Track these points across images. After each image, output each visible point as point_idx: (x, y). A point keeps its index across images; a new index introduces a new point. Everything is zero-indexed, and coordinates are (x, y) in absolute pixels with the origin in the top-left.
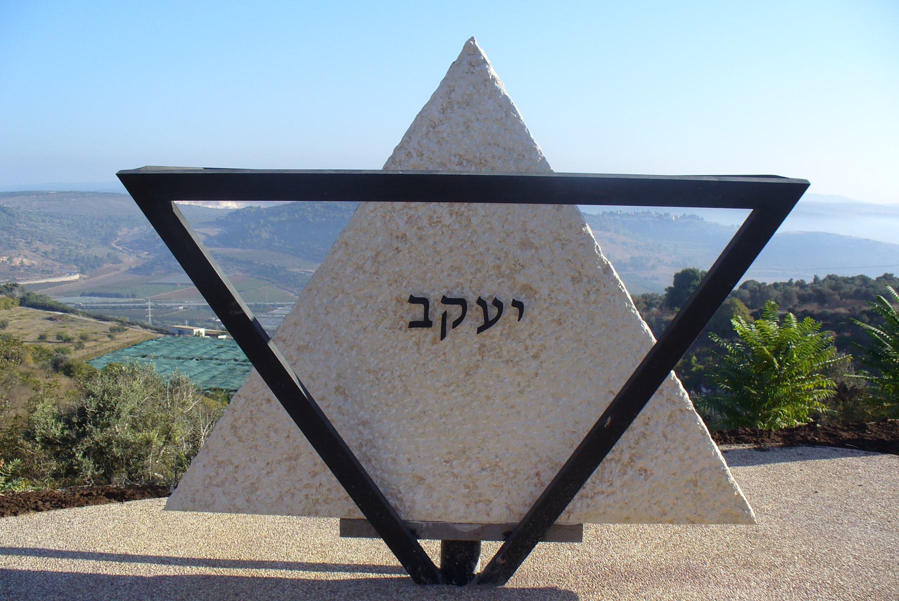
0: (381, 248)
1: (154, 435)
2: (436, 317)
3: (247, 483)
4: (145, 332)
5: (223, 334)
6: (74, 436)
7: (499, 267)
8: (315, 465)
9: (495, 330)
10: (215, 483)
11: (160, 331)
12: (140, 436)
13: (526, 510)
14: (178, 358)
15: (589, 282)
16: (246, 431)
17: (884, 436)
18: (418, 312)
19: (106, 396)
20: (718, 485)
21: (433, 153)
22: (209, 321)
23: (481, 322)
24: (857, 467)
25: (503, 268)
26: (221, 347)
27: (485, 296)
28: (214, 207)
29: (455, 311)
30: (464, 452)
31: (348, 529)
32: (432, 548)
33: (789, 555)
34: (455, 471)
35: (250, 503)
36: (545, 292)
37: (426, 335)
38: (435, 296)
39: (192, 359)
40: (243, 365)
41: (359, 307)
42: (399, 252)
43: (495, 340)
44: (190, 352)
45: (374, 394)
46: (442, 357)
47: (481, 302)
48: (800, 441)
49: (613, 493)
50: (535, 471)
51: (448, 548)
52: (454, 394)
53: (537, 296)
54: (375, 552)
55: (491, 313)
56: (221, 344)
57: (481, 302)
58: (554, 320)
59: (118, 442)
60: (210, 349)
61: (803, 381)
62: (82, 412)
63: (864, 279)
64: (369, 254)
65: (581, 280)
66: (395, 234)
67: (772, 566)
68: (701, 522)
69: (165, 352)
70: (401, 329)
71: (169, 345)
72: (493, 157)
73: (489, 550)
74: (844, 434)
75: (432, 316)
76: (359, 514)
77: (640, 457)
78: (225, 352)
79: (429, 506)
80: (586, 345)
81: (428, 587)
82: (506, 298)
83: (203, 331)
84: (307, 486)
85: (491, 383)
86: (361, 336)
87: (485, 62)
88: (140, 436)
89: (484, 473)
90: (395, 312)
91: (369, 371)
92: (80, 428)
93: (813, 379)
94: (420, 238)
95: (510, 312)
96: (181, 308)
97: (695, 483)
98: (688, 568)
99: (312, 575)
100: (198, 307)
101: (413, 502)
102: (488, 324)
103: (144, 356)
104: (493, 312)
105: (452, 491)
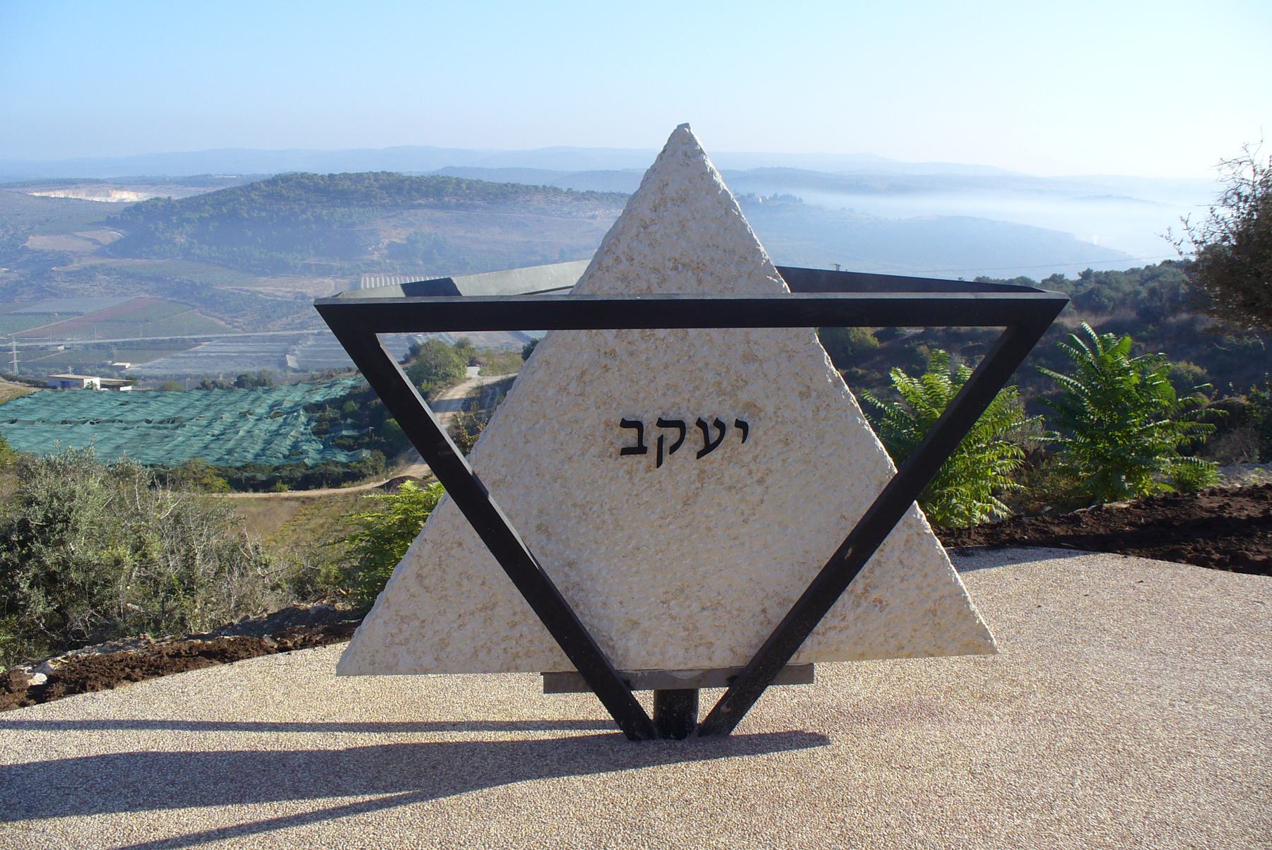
0: (586, 366)
1: (124, 552)
2: (651, 442)
3: (437, 639)
4: (12, 385)
5: (126, 384)
6: (17, 560)
7: (720, 383)
8: (515, 614)
9: (716, 455)
10: (397, 641)
11: (36, 384)
12: (105, 554)
13: (753, 652)
14: (64, 422)
15: (818, 397)
16: (434, 580)
17: (1102, 530)
18: (631, 436)
19: (55, 503)
20: (959, 613)
21: (645, 256)
22: (104, 365)
23: (700, 446)
24: (1079, 573)
25: (725, 384)
26: (126, 403)
27: (705, 416)
28: (103, 200)
29: (672, 435)
30: (682, 591)
31: (554, 684)
32: (645, 699)
33: (1026, 683)
34: (673, 612)
35: (439, 661)
36: (770, 409)
37: (639, 462)
38: (649, 419)
39: (84, 423)
40: (159, 428)
41: (563, 433)
42: (607, 370)
43: (716, 465)
44: (80, 413)
45: (582, 531)
46: (658, 486)
47: (701, 424)
48: (1006, 541)
49: (846, 628)
50: (761, 607)
51: (662, 699)
52: (672, 527)
53: (762, 414)
54: (587, 707)
55: (712, 435)
56: (125, 399)
57: (701, 424)
58: (780, 440)
59: (76, 564)
60: (111, 408)
61: (983, 450)
62: (24, 525)
63: (1024, 286)
64: (573, 373)
65: (809, 396)
66: (602, 351)
67: (1011, 699)
68: (941, 654)
69: (44, 414)
70: (610, 456)
71: (49, 403)
72: (713, 260)
73: (708, 700)
74: (1056, 529)
75: (646, 440)
76: (567, 665)
77: (875, 587)
78: (132, 410)
79: (644, 653)
80: (815, 466)
81: (644, 743)
82: (729, 418)
83: (97, 381)
84: (507, 638)
85: (712, 512)
86: (566, 467)
87: (701, 152)
88: (105, 554)
89: (705, 613)
90: (604, 438)
91: (575, 505)
92: (22, 549)
93: (994, 447)
94: (631, 354)
95: (733, 433)
96: (62, 348)
97: (934, 612)
98: (921, 706)
99: (472, 736)
100: (86, 346)
101: (627, 650)
102: (709, 448)
103: (13, 422)
104: (714, 434)
105: (670, 635)
